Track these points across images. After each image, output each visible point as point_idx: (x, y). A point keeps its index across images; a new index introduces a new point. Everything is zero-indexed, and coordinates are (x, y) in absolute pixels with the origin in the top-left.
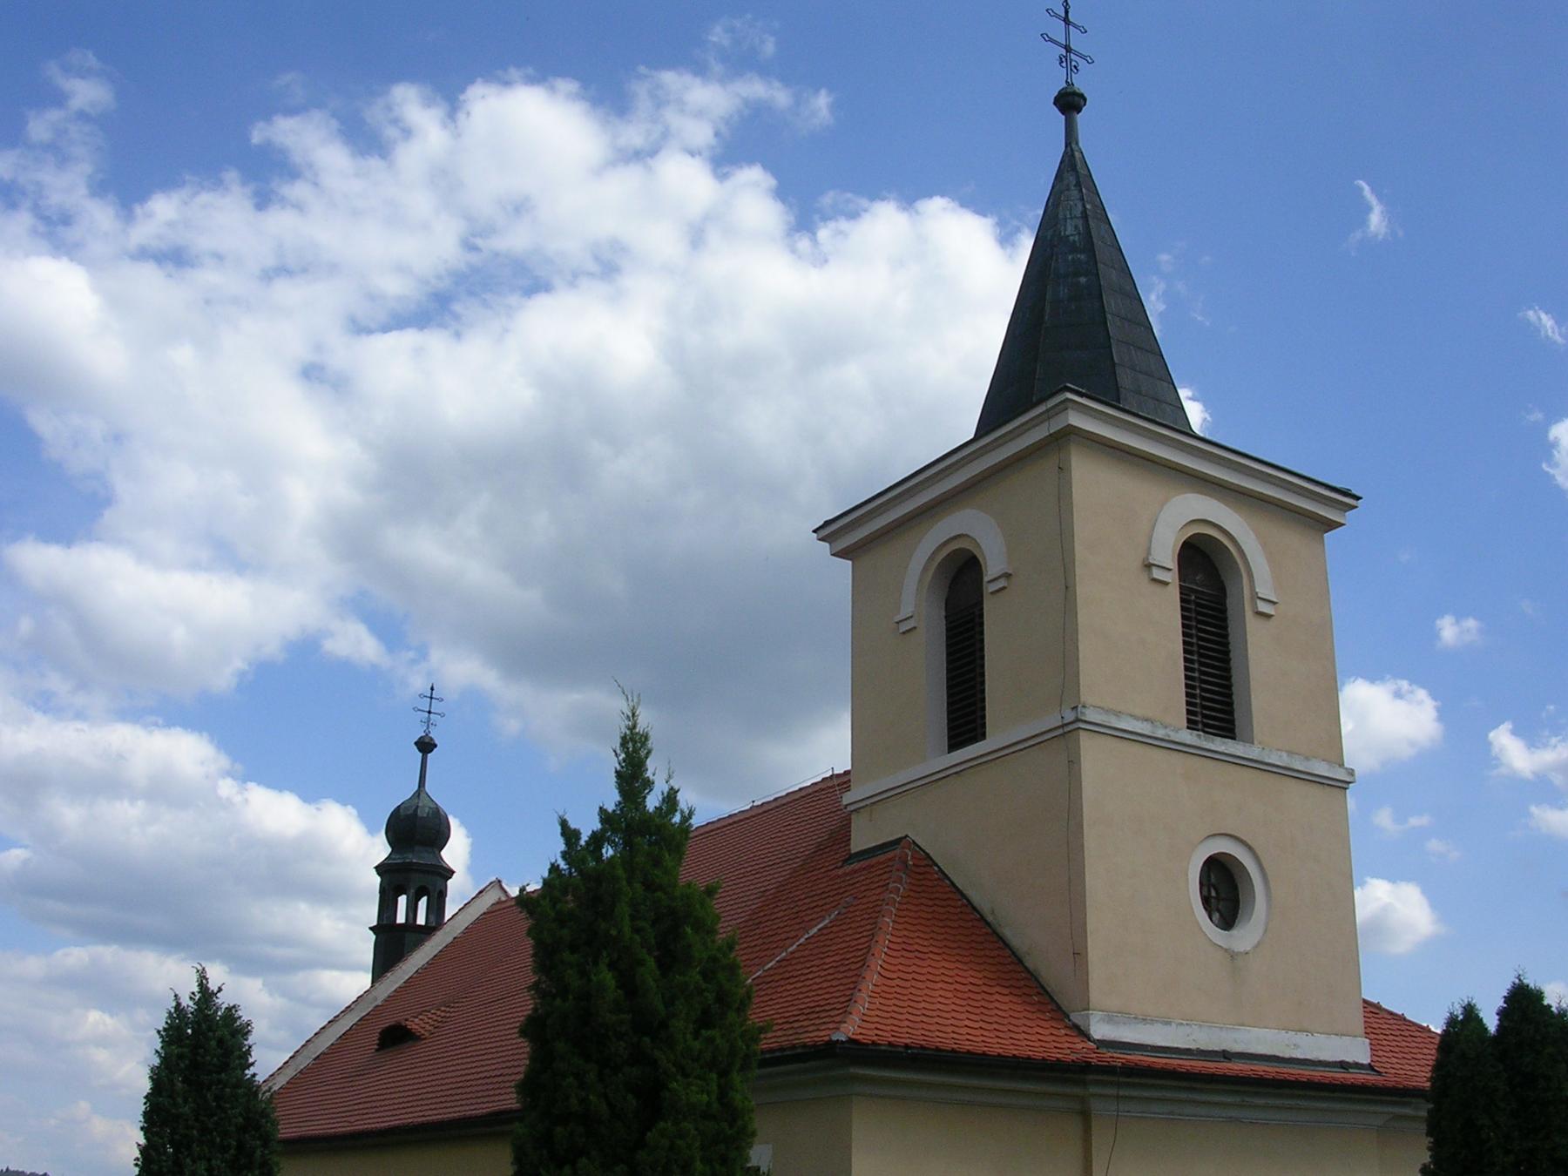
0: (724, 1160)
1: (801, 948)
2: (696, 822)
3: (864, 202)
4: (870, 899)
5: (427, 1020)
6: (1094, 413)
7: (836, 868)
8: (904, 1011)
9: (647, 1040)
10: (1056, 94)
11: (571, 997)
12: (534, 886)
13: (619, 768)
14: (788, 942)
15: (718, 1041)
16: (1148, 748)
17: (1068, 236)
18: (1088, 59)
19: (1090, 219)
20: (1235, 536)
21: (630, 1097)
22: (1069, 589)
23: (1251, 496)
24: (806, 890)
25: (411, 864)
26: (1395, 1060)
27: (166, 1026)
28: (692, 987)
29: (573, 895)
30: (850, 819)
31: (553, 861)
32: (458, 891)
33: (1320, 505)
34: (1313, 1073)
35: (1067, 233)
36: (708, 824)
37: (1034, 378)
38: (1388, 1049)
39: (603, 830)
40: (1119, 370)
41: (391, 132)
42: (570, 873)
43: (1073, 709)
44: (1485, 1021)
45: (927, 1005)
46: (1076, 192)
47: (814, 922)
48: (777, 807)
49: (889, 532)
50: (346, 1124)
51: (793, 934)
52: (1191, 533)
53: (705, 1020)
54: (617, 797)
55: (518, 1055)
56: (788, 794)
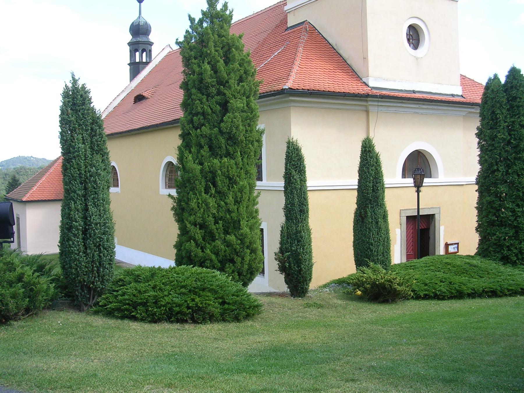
0: (249, 125)
5: (149, 92)
9: (222, 87)
15: (246, 86)
21: (217, 106)
26: (470, 94)
27: (63, 92)
32: (155, 50)
34: (442, 98)
38: (468, 90)
39: (203, 18)
44: (500, 79)
45: (315, 76)
47: (275, 51)
50: (126, 128)
51: (269, 55)
53: (241, 80)
54: (207, 6)
55: (180, 95)
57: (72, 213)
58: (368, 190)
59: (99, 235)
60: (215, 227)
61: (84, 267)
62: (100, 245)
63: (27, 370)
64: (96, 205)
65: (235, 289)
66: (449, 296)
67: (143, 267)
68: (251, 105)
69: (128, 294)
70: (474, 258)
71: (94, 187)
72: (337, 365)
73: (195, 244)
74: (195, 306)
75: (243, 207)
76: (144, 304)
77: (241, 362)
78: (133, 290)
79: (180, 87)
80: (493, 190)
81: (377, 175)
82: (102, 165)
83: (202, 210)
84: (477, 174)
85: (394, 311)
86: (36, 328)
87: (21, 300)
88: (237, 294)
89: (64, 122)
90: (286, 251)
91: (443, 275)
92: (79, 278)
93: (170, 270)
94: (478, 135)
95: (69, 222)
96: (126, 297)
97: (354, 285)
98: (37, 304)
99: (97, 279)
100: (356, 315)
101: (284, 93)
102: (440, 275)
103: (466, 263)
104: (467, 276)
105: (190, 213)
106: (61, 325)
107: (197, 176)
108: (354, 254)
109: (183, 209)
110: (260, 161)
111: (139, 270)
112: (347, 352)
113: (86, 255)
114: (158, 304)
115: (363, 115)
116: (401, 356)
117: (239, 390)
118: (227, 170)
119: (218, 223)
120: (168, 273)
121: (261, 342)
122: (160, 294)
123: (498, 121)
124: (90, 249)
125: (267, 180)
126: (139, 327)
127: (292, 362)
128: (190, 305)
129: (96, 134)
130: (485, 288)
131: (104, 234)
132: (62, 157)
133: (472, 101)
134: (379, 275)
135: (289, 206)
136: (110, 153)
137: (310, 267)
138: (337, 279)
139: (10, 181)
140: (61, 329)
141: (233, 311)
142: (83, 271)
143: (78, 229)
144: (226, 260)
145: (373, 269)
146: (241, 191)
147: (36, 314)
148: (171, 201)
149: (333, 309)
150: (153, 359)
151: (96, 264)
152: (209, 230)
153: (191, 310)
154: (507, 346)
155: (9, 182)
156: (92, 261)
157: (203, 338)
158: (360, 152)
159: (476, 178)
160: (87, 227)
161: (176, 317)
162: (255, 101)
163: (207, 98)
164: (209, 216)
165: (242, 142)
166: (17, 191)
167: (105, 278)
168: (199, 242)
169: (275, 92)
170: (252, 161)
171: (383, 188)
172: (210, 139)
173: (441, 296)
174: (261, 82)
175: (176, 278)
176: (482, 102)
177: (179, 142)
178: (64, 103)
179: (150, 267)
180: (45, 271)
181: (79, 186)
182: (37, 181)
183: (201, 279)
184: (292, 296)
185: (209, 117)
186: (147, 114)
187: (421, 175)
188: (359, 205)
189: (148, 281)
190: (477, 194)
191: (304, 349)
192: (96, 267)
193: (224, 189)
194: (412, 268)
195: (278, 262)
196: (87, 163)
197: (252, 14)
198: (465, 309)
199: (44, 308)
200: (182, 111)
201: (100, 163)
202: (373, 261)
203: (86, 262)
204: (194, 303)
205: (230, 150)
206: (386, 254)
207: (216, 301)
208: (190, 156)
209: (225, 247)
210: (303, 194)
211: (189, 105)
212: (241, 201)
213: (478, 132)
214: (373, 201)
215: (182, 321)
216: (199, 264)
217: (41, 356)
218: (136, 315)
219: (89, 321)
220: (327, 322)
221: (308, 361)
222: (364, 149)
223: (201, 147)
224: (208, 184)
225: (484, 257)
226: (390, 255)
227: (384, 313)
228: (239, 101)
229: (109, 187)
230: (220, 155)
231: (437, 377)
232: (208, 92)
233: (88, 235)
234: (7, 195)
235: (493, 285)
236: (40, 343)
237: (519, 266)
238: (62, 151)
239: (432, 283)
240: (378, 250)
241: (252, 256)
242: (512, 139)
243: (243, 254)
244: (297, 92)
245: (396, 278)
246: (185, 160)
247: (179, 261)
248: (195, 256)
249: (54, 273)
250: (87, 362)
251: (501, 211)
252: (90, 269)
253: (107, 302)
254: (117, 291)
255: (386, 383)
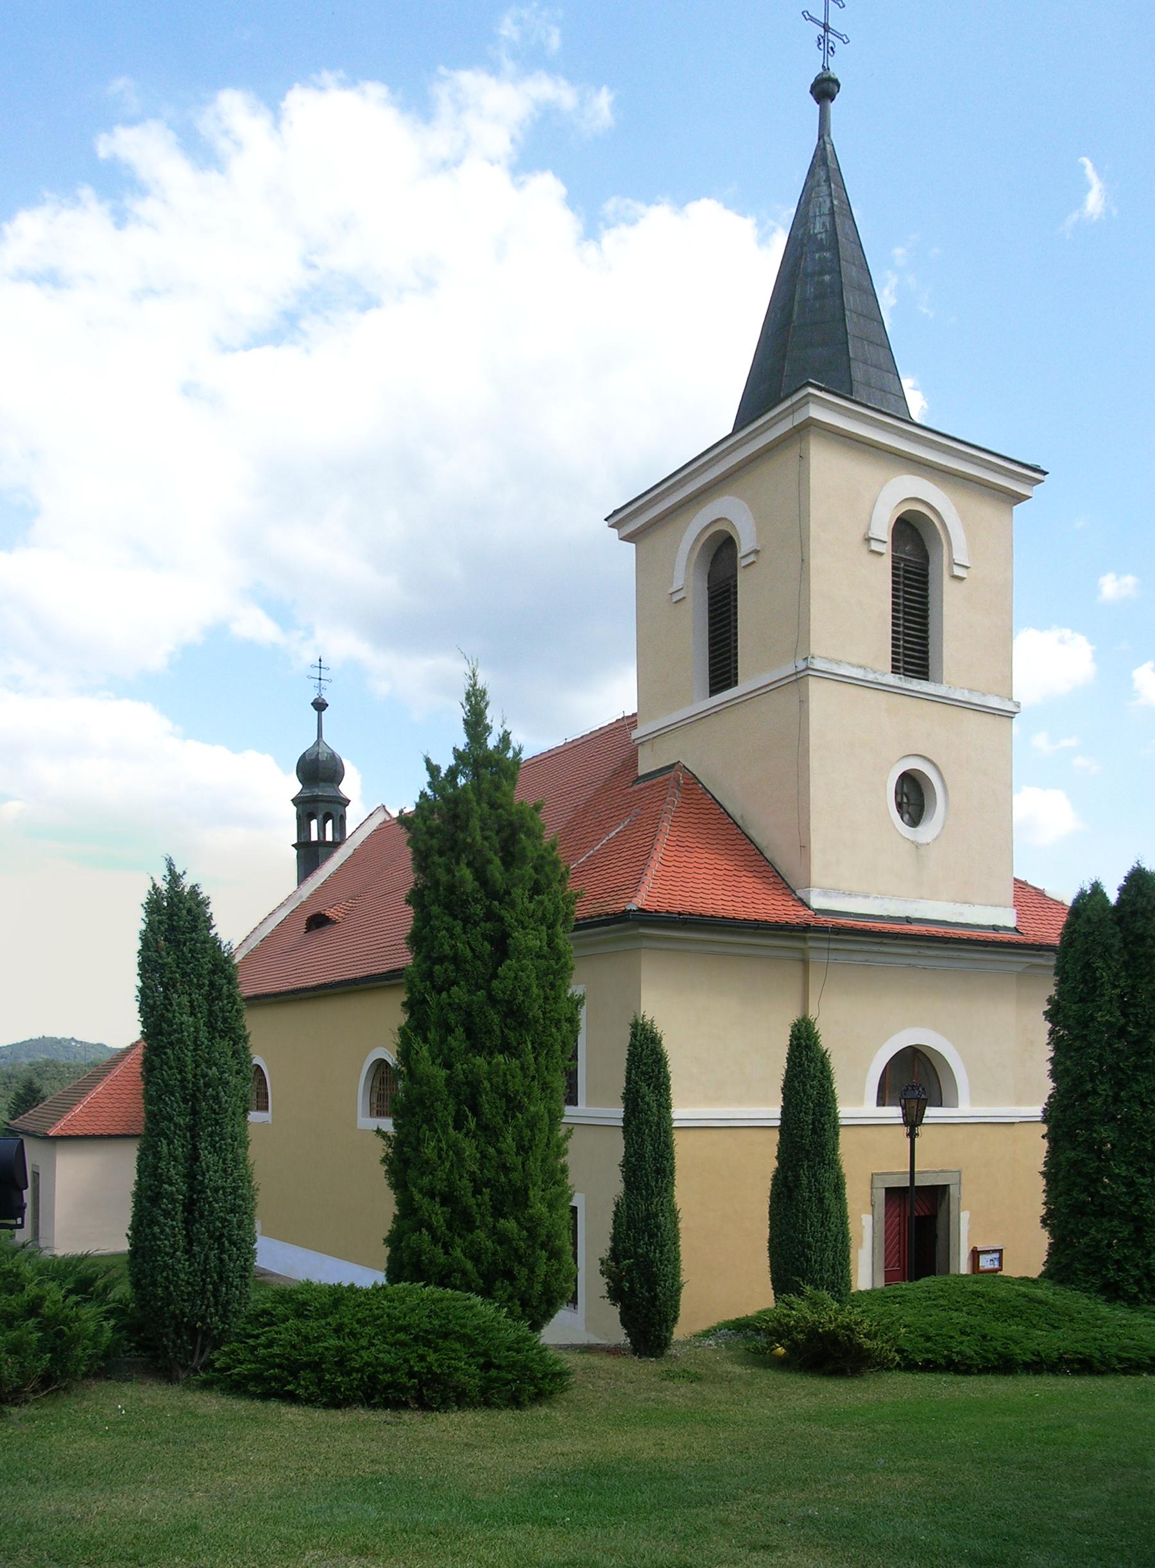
0: (552, 986)
1: (604, 847)
2: (524, 756)
3: (641, 208)
4: (653, 810)
5: (339, 910)
6: (830, 406)
7: (628, 787)
8: (677, 889)
9: (496, 903)
10: (813, 80)
11: (441, 888)
12: (410, 808)
13: (465, 717)
14: (595, 842)
15: (546, 903)
16: (860, 690)
17: (816, 234)
18: (844, 38)
19: (836, 216)
20: (939, 510)
21: (486, 943)
22: (804, 561)
23: (955, 475)
24: (606, 804)
25: (318, 796)
26: (1034, 925)
28: (527, 877)
29: (438, 814)
30: (637, 750)
31: (422, 789)
32: (354, 816)
33: (1013, 481)
35: (816, 231)
36: (533, 757)
37: (782, 375)
38: (1030, 917)
39: (457, 765)
40: (853, 364)
41: (224, 145)
42: (435, 798)
43: (804, 659)
44: (1108, 895)
46: (825, 188)
48: (584, 743)
49: (664, 518)
51: (598, 837)
52: (904, 510)
53: (536, 889)
54: (466, 740)
55: (405, 919)
56: (591, 733)
57: (162, 1164)
58: (803, 1130)
59: (222, 1214)
60: (475, 1202)
61: (183, 1283)
62: (222, 1235)
63: (34, 1520)
64: (216, 1150)
65: (513, 1336)
66: (981, 1367)
67: (315, 1284)
68: (557, 943)
69: (281, 1343)
70: (1038, 1284)
71: (215, 1110)
72: (732, 1510)
73: (430, 1236)
74: (425, 1371)
75: (536, 1159)
76: (315, 1366)
77: (522, 1499)
78: (291, 1336)
79: (406, 900)
80: (1083, 1136)
81: (823, 1099)
82: (233, 1063)
83: (448, 1164)
84: (1046, 1101)
85: (858, 1395)
86: (64, 1421)
87: (31, 1357)
88: (518, 1345)
89: (149, 965)
90: (623, 1256)
91: (966, 1319)
92: (172, 1307)
93: (374, 1292)
94: (1050, 1016)
95: (154, 1184)
96: (276, 1350)
97: (771, 1335)
98: (71, 1367)
99: (213, 1310)
100: (773, 1400)
101: (628, 920)
102: (960, 1318)
103: (1019, 1295)
104: (1023, 1322)
105: (422, 1170)
106: (124, 1412)
107: (439, 1092)
108: (771, 1266)
109: (406, 1162)
110: (573, 1062)
111: (307, 1291)
112: (753, 1481)
113: (190, 1257)
114: (346, 1366)
115: (798, 969)
116: (873, 1496)
117: (516, 1562)
118: (504, 1081)
119: (481, 1193)
120: (369, 1299)
121: (567, 1455)
122: (350, 1343)
123: (1098, 984)
124: (200, 1243)
125: (588, 1104)
126: (301, 1418)
127: (633, 1501)
128: (416, 1369)
129: (220, 995)
130: (1065, 1353)
131: (232, 1211)
132: (143, 1043)
133: (1039, 940)
134: (824, 1313)
135: (634, 1159)
136: (250, 1038)
137: (675, 1292)
138: (734, 1319)
139: (21, 1092)
140: (122, 1423)
141: (508, 1382)
142: (182, 1291)
143: (173, 1201)
144: (496, 1273)
145: (811, 1299)
146: (532, 1125)
147: (65, 1389)
148: (381, 1143)
149: (724, 1386)
150: (329, 1488)
151: (211, 1277)
152: (462, 1207)
153: (416, 1381)
154: (1122, 1489)
155: (18, 1094)
156: (202, 1271)
157: (440, 1442)
158: (787, 1048)
159: (1044, 1109)
160: (195, 1196)
161: (384, 1396)
162: (566, 936)
163: (463, 926)
164: (461, 1177)
165: (537, 1022)
166: (35, 1114)
167: (230, 1308)
168: (438, 1234)
169: (609, 917)
170: (557, 1063)
171: (835, 1127)
172: (469, 1014)
173: (963, 1364)
174: (578, 894)
175: (387, 1310)
176: (1062, 942)
177: (402, 1018)
178: (149, 924)
179: (332, 1284)
180: (93, 1291)
181: (180, 1107)
182: (84, 1094)
183: (440, 1314)
184: (635, 1355)
185: (468, 967)
186: (334, 956)
187: (918, 1099)
188: (783, 1160)
189: (326, 1316)
190: (1045, 1144)
191: (660, 1471)
192: (210, 1283)
193: (495, 1120)
194: (898, 1300)
195: (607, 1280)
196: (200, 1057)
197: (562, 744)
198: (1019, 1397)
199: (86, 1376)
200: (410, 951)
201: (228, 1059)
202: (812, 1282)
203: (190, 1273)
204: (423, 1364)
205: (510, 1039)
206: (839, 1268)
207: (471, 1360)
208: (425, 1048)
209: (495, 1244)
210: (662, 1134)
211: (425, 939)
212: (530, 1148)
213: (1050, 1009)
214: (813, 1154)
215: (397, 1405)
216: (437, 1281)
217: (70, 1486)
218: (296, 1390)
219: (190, 1404)
220: (709, 1415)
221: (669, 1499)
222: (795, 1043)
223: (450, 1030)
224: (461, 1110)
225: (1061, 1282)
226: (849, 1271)
227: (836, 1398)
228: (532, 934)
229: (246, 1111)
230: (489, 1048)
231: (958, 1549)
232: (465, 912)
233: (196, 1214)
234: (12, 1122)
235: (1084, 1347)
236: (70, 1456)
237: (1145, 1306)
238: (142, 1029)
239: (941, 1335)
240: (821, 1259)
241: (553, 1265)
242: (1131, 1025)
243: (531, 1260)
244: (655, 918)
245: (862, 1320)
246: (415, 1056)
247: (394, 1275)
248: (431, 1262)
249: (114, 1296)
250: (179, 1498)
251: (1102, 1182)
252: (197, 1288)
253: (233, 1362)
254: (257, 1337)
255: (841, 1557)
